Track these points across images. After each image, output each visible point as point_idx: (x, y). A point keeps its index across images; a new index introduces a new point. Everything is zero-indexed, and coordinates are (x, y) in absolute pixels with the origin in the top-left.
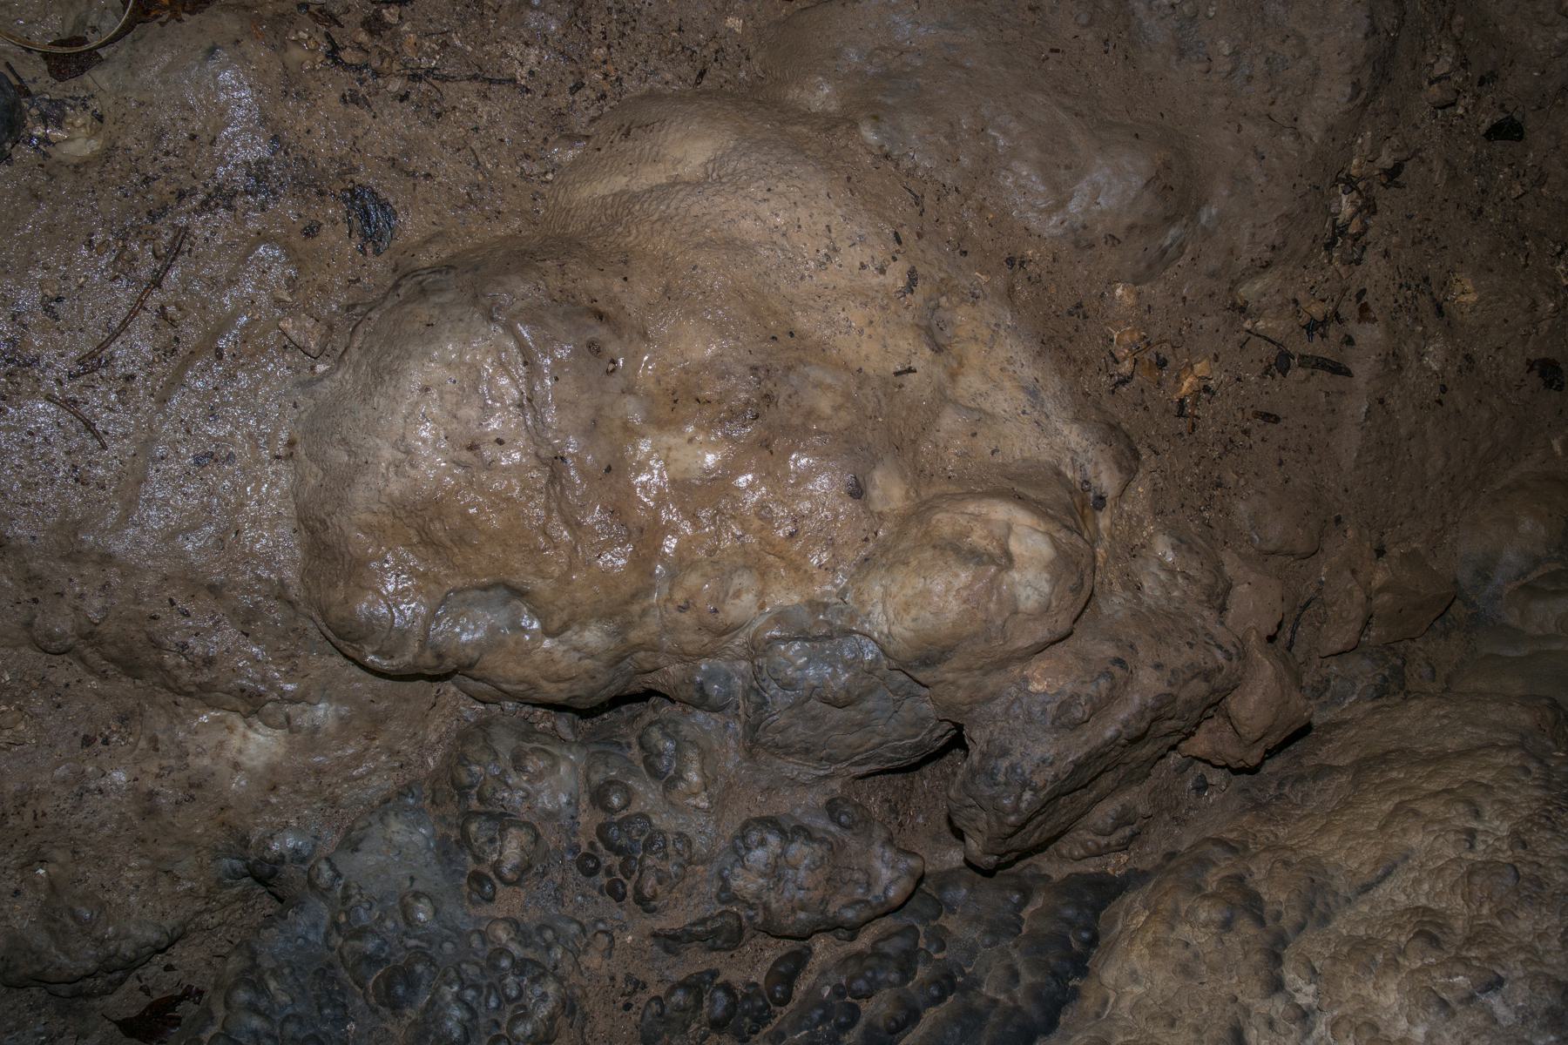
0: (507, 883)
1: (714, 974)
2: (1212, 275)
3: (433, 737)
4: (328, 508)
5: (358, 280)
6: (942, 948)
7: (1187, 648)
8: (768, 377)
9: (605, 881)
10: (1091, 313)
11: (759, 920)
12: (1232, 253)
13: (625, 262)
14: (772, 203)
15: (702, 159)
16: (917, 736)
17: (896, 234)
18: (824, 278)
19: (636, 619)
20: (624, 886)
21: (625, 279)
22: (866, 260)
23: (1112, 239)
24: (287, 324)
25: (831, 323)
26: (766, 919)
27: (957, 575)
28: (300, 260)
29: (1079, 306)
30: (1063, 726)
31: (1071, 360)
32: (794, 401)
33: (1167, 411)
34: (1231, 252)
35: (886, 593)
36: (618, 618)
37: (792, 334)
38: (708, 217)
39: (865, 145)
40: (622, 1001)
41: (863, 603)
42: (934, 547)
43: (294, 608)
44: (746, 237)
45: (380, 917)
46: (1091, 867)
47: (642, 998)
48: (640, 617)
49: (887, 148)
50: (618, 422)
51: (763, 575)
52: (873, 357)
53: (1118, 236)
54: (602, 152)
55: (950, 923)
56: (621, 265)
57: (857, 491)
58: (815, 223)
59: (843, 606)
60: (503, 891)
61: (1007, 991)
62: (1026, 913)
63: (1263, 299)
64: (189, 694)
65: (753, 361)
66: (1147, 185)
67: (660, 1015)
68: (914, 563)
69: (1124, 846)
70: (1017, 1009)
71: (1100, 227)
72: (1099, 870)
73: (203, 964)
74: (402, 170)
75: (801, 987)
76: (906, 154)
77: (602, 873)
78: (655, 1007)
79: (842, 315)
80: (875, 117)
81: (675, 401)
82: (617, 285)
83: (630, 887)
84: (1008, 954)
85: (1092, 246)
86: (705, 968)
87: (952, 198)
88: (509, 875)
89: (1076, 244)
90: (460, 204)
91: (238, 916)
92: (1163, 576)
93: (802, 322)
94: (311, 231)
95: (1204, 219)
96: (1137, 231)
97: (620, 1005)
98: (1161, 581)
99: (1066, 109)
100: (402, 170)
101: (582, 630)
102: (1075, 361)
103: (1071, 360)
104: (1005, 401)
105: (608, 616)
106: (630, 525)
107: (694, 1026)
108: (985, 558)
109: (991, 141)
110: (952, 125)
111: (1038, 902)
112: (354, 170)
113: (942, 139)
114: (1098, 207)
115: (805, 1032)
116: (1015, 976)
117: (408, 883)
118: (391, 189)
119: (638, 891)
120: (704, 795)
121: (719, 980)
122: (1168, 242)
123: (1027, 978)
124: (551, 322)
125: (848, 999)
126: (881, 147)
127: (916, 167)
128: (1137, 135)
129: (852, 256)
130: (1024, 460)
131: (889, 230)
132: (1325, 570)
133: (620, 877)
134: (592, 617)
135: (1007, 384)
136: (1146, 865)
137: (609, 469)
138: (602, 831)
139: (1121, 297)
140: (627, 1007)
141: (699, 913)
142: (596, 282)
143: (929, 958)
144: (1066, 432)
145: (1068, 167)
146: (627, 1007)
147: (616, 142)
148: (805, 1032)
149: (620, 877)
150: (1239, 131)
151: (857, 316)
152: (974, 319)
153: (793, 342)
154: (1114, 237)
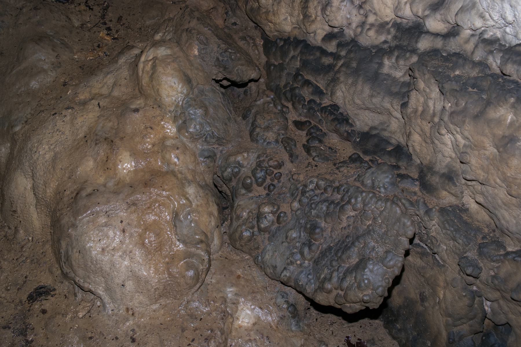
0: (279, 208)
1: (304, 145)
2: (71, 32)
3: (239, 257)
4: (150, 287)
5: (65, 295)
6: (289, 83)
7: (185, 18)
8: (99, 140)
9: (276, 181)
10: (83, 64)
11: (283, 132)
12: (64, 27)
13: (59, 193)
14: (40, 150)
15: (25, 180)
16: (219, 93)
17: (53, 115)
18: (67, 132)
19: (183, 176)
20: (276, 173)
21: (65, 191)
22: (61, 121)
23: (57, 56)
24: (81, 315)
25: (82, 127)
26: (283, 130)
27: (160, 72)
28: (55, 314)
29: (80, 67)
30: (207, 42)
31: (98, 67)
32: (107, 132)
33: (115, 42)
34: (63, 27)
35: (168, 96)
36: (184, 181)
37: (85, 137)
38: (45, 169)
39: (21, 129)
40: (314, 168)
41: (173, 103)
42: (152, 81)
43: (189, 302)
44: (52, 156)
45: (296, 249)
46: (261, 49)
47: (314, 163)
48: (183, 174)
49: (23, 122)
50: (116, 187)
51: (166, 138)
52: (94, 114)
53: (56, 55)
54: (21, 220)
55: (282, 84)
56: (60, 194)
57: (137, 110)
58: (48, 137)
59: (175, 111)
60: (282, 209)
61: (297, 58)
62: (276, 63)
63: (80, 20)
64: (226, 339)
65: (93, 146)
66: (39, 45)
67: (318, 156)
68: (158, 87)
69: (254, 40)
70: (301, 52)
71: (53, 60)
72: (262, 47)
73: (336, 338)
74: (23, 285)
75: (304, 119)
76: (26, 116)
77: (273, 183)
78: (316, 159)
79: (79, 124)
80: (12, 127)
81: (108, 168)
82: (68, 192)
83: (276, 171)
84: (288, 63)
85: (60, 63)
86: (302, 148)
87: (42, 103)
88: (276, 207)
89: (59, 67)
90: (38, 265)
91: (316, 328)
92: (166, 34)
93: (81, 135)
94: (44, 312)
95: (51, 34)
96: (54, 49)
97: (316, 168)
98: (168, 34)
99: (12, 71)
100: (23, 285)
101: (188, 194)
102: (98, 66)
103: (98, 67)
104: (110, 80)
105: (183, 185)
106: (150, 178)
107: (322, 148)
108: (154, 64)
109: (22, 92)
110: (16, 104)
111: (273, 61)
112: (21, 302)
113: (20, 106)
114: (46, 59)
115: (318, 113)
116: (293, 57)
117: (284, 244)
118: (30, 288)
119: (275, 167)
120: (243, 154)
121: (306, 143)
122: (59, 42)
123: (292, 53)
124: (78, 208)
125: (306, 103)
126: (23, 124)
127: (30, 113)
128: (21, 49)
129: (60, 124)
130: (128, 71)
131: (52, 117)
132: (168, 2)
133: (273, 175)
134: (183, 190)
135: (105, 81)
136: (259, 35)
137: (131, 187)
138: (260, 185)
139: (78, 56)
140: (316, 166)
141: (283, 150)
142: (65, 199)
143: (292, 85)
144: (120, 63)
145: (32, 69)
146: (316, 166)
147: (18, 215)
148: (318, 113)
149: (273, 175)
150: (21, 24)
151: (80, 120)
152: (83, 93)
153: (88, 136)
154: (57, 56)
